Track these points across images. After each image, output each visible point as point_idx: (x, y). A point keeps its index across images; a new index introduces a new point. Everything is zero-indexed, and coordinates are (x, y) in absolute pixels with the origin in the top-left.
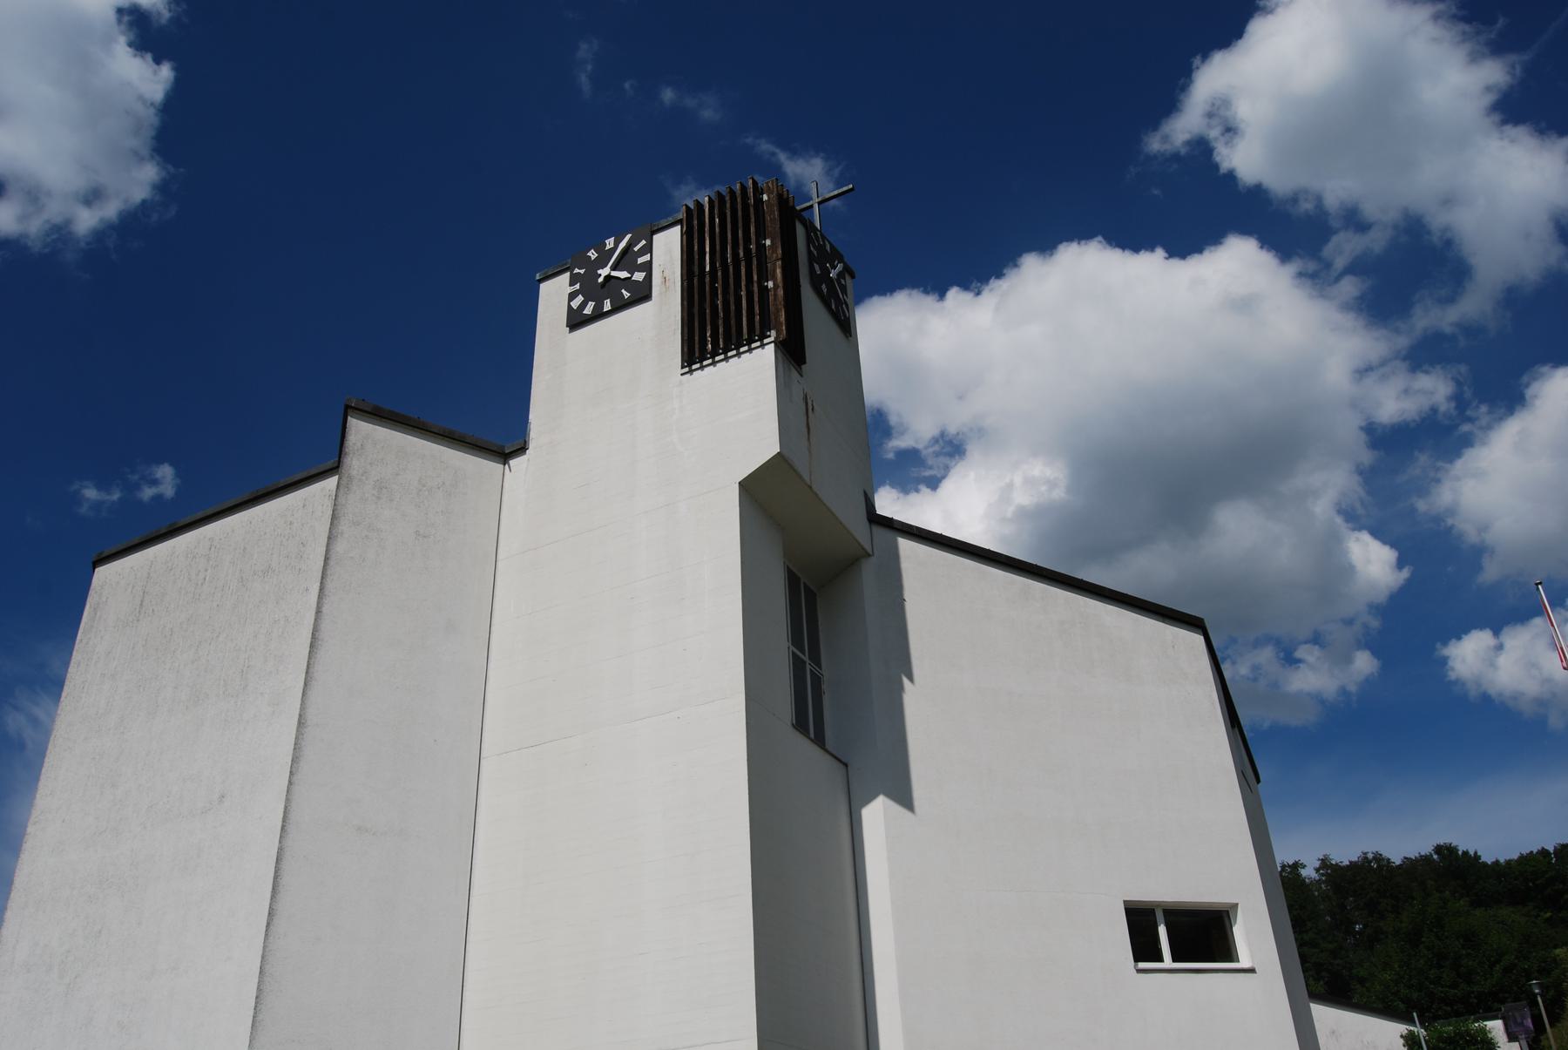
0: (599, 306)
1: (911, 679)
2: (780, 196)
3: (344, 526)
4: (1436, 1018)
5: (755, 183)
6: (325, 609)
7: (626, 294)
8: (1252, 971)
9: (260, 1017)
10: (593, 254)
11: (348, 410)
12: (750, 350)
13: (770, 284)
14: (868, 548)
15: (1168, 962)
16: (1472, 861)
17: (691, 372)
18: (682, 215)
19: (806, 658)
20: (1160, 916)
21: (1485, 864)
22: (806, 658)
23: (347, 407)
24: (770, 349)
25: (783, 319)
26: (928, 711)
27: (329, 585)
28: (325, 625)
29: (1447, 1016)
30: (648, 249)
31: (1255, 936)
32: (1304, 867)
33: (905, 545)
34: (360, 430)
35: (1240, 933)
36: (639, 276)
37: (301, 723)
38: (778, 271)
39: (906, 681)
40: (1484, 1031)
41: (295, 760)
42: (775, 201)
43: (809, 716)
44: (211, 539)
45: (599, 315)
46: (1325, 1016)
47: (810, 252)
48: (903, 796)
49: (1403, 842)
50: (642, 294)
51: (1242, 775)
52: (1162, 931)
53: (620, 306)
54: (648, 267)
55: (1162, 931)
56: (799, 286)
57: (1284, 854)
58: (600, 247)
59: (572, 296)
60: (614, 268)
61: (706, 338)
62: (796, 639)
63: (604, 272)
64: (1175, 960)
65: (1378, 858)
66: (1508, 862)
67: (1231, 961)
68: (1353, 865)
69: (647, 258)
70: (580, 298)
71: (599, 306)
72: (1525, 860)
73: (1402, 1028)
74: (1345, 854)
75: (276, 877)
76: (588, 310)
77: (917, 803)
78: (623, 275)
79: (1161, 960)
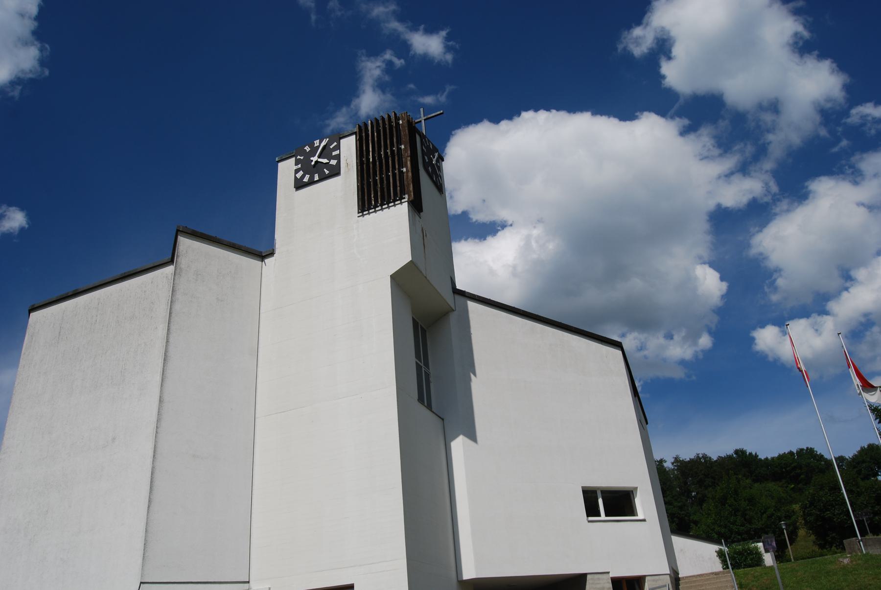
0: (312, 177)
1: (475, 375)
2: (408, 121)
3: (179, 296)
4: (733, 542)
5: (395, 114)
6: (171, 340)
7: (327, 172)
8: (644, 520)
9: (147, 554)
10: (307, 149)
11: (178, 232)
12: (395, 205)
13: (404, 170)
14: (453, 306)
15: (603, 516)
16: (754, 458)
17: (363, 215)
18: (356, 130)
19: (422, 365)
20: (599, 494)
21: (760, 460)
22: (422, 365)
23: (178, 231)
24: (405, 205)
25: (411, 189)
26: (483, 390)
27: (173, 327)
28: (171, 348)
29: (739, 541)
30: (338, 147)
31: (646, 503)
32: (665, 462)
33: (472, 305)
34: (185, 243)
35: (638, 502)
36: (333, 162)
37: (161, 401)
38: (409, 163)
39: (472, 376)
40: (756, 548)
41: (159, 420)
42: (406, 125)
43: (424, 396)
44: (99, 299)
45: (312, 182)
46: (678, 541)
47: (422, 150)
48: (472, 435)
49: (717, 445)
50: (335, 172)
51: (640, 422)
52: (600, 501)
53: (321, 179)
54: (338, 157)
55: (600, 501)
56: (418, 170)
57: (657, 457)
58: (311, 145)
59: (297, 171)
60: (319, 157)
61: (370, 198)
62: (418, 356)
63: (314, 159)
64: (607, 515)
65: (705, 457)
66: (773, 459)
67: (634, 515)
68: (691, 461)
69: (337, 152)
70: (301, 173)
71: (312, 177)
72: (781, 457)
73: (716, 547)
74: (687, 454)
75: (152, 482)
76: (306, 179)
77: (479, 439)
78: (325, 161)
79: (599, 515)
